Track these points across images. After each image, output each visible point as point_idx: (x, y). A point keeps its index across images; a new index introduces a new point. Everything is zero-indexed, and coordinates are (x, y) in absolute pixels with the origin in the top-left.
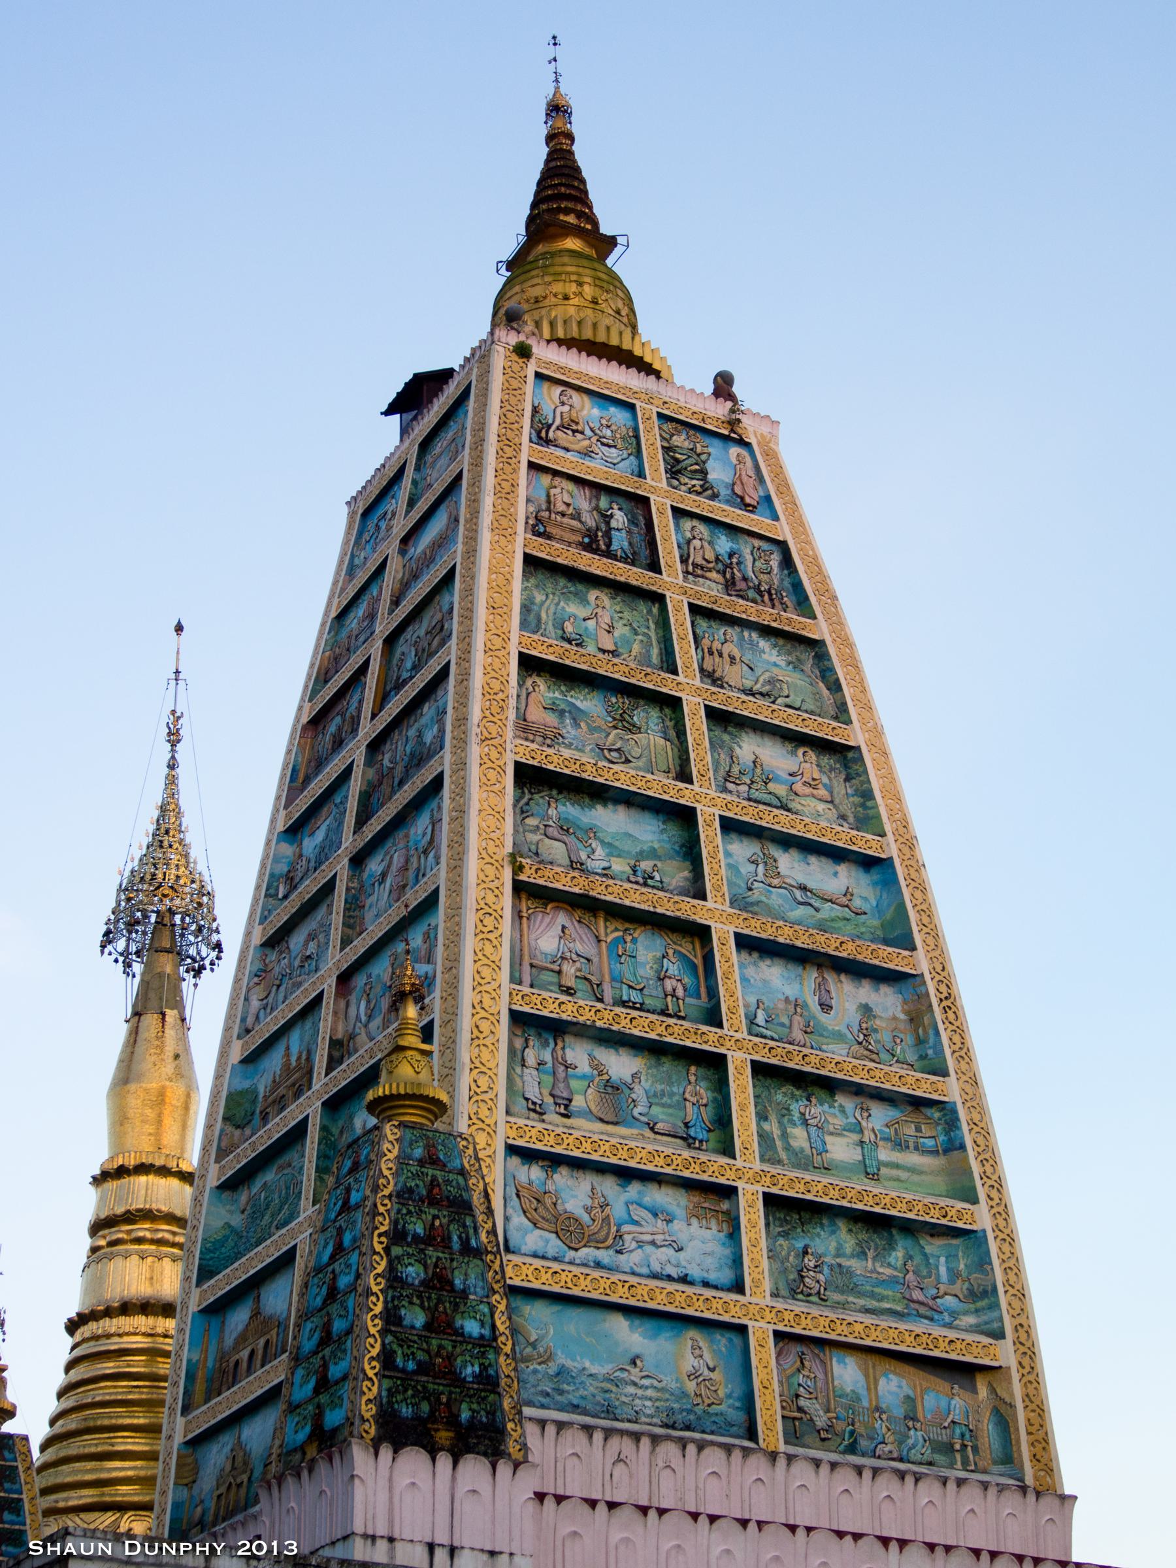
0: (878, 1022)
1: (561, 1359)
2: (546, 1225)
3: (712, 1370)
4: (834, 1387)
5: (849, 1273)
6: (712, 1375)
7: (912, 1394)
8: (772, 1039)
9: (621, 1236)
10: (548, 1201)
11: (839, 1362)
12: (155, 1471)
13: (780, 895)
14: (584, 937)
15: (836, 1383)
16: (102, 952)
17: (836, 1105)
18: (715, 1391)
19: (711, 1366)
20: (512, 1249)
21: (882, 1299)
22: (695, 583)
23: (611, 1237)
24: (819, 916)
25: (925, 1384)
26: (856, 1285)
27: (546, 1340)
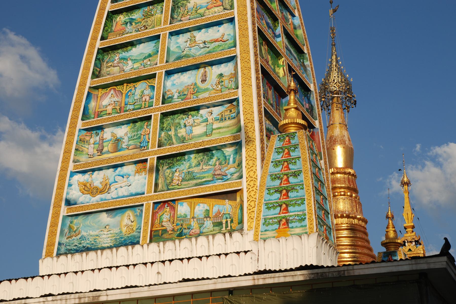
0: (224, 78)
1: (84, 233)
2: (86, 192)
3: (132, 222)
4: (177, 215)
5: (192, 172)
6: (132, 224)
7: (208, 209)
8: (410, 254)
9: (110, 188)
10: (88, 185)
11: (180, 206)
12: (336, 232)
13: (195, 49)
14: (118, 95)
15: (178, 213)
16: (419, 236)
17: (199, 115)
18: (133, 229)
19: (132, 221)
20: (72, 202)
21: (204, 177)
22: (258, 61)
23: (107, 189)
24: (209, 49)
25: (214, 203)
26: (194, 177)
27: (79, 228)
